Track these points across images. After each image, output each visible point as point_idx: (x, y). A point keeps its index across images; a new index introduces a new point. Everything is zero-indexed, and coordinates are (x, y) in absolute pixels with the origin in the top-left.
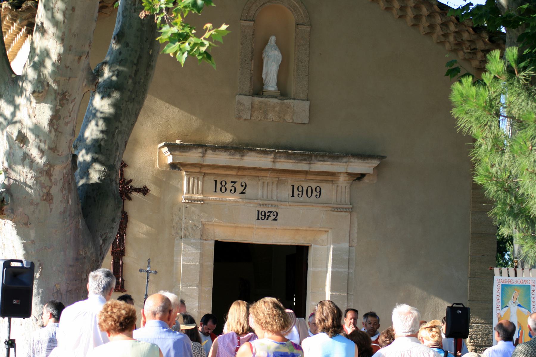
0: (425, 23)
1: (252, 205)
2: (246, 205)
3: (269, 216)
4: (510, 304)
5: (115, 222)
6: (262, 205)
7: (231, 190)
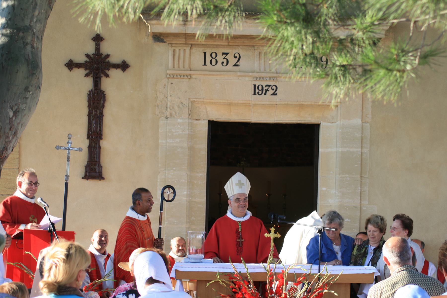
1: (247, 78)
2: (240, 78)
3: (267, 90)
5: (29, 91)
6: (258, 79)
7: (223, 63)
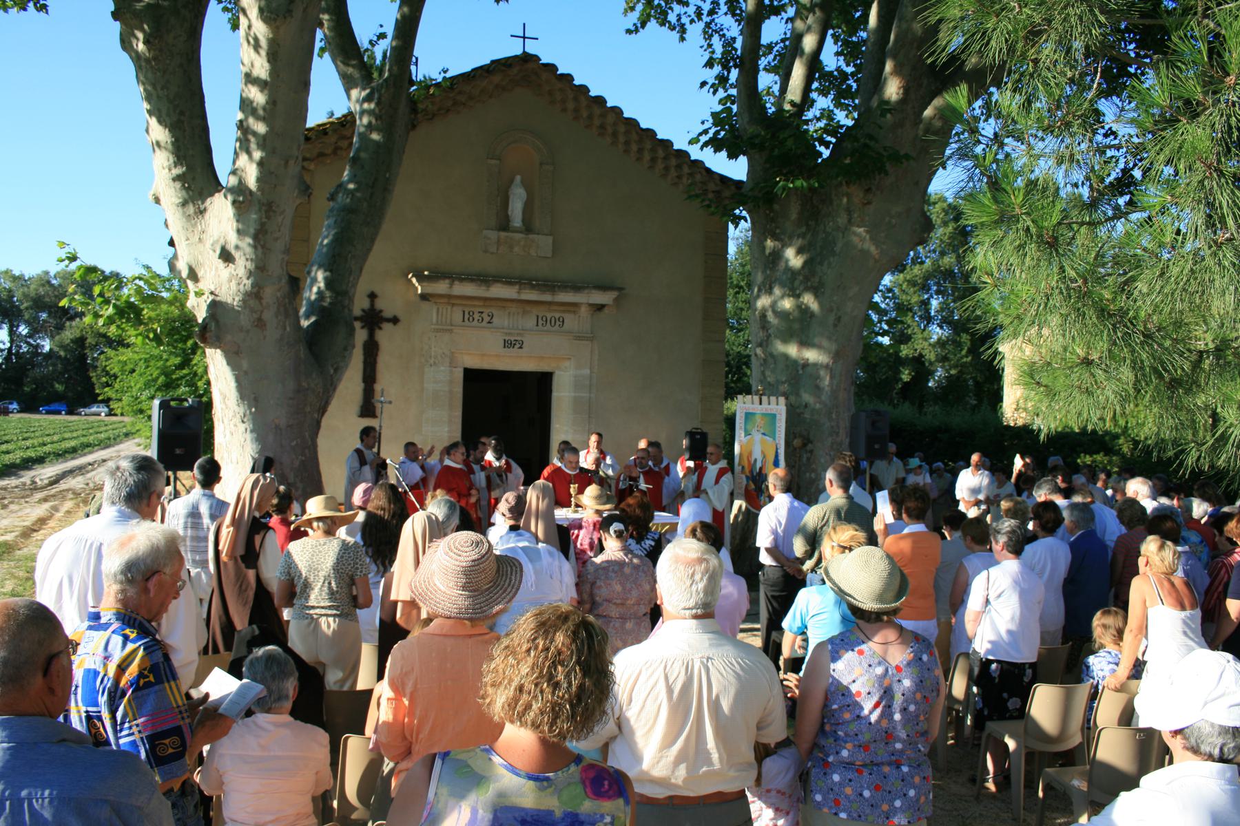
0: (660, 165)
4: (754, 432)
